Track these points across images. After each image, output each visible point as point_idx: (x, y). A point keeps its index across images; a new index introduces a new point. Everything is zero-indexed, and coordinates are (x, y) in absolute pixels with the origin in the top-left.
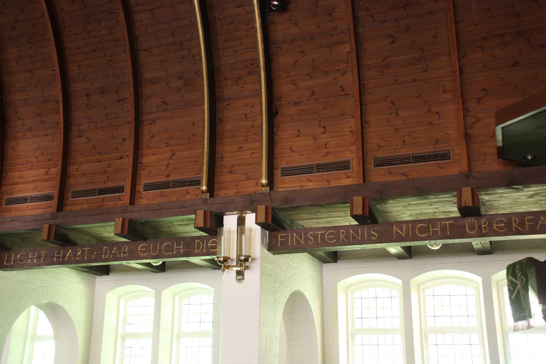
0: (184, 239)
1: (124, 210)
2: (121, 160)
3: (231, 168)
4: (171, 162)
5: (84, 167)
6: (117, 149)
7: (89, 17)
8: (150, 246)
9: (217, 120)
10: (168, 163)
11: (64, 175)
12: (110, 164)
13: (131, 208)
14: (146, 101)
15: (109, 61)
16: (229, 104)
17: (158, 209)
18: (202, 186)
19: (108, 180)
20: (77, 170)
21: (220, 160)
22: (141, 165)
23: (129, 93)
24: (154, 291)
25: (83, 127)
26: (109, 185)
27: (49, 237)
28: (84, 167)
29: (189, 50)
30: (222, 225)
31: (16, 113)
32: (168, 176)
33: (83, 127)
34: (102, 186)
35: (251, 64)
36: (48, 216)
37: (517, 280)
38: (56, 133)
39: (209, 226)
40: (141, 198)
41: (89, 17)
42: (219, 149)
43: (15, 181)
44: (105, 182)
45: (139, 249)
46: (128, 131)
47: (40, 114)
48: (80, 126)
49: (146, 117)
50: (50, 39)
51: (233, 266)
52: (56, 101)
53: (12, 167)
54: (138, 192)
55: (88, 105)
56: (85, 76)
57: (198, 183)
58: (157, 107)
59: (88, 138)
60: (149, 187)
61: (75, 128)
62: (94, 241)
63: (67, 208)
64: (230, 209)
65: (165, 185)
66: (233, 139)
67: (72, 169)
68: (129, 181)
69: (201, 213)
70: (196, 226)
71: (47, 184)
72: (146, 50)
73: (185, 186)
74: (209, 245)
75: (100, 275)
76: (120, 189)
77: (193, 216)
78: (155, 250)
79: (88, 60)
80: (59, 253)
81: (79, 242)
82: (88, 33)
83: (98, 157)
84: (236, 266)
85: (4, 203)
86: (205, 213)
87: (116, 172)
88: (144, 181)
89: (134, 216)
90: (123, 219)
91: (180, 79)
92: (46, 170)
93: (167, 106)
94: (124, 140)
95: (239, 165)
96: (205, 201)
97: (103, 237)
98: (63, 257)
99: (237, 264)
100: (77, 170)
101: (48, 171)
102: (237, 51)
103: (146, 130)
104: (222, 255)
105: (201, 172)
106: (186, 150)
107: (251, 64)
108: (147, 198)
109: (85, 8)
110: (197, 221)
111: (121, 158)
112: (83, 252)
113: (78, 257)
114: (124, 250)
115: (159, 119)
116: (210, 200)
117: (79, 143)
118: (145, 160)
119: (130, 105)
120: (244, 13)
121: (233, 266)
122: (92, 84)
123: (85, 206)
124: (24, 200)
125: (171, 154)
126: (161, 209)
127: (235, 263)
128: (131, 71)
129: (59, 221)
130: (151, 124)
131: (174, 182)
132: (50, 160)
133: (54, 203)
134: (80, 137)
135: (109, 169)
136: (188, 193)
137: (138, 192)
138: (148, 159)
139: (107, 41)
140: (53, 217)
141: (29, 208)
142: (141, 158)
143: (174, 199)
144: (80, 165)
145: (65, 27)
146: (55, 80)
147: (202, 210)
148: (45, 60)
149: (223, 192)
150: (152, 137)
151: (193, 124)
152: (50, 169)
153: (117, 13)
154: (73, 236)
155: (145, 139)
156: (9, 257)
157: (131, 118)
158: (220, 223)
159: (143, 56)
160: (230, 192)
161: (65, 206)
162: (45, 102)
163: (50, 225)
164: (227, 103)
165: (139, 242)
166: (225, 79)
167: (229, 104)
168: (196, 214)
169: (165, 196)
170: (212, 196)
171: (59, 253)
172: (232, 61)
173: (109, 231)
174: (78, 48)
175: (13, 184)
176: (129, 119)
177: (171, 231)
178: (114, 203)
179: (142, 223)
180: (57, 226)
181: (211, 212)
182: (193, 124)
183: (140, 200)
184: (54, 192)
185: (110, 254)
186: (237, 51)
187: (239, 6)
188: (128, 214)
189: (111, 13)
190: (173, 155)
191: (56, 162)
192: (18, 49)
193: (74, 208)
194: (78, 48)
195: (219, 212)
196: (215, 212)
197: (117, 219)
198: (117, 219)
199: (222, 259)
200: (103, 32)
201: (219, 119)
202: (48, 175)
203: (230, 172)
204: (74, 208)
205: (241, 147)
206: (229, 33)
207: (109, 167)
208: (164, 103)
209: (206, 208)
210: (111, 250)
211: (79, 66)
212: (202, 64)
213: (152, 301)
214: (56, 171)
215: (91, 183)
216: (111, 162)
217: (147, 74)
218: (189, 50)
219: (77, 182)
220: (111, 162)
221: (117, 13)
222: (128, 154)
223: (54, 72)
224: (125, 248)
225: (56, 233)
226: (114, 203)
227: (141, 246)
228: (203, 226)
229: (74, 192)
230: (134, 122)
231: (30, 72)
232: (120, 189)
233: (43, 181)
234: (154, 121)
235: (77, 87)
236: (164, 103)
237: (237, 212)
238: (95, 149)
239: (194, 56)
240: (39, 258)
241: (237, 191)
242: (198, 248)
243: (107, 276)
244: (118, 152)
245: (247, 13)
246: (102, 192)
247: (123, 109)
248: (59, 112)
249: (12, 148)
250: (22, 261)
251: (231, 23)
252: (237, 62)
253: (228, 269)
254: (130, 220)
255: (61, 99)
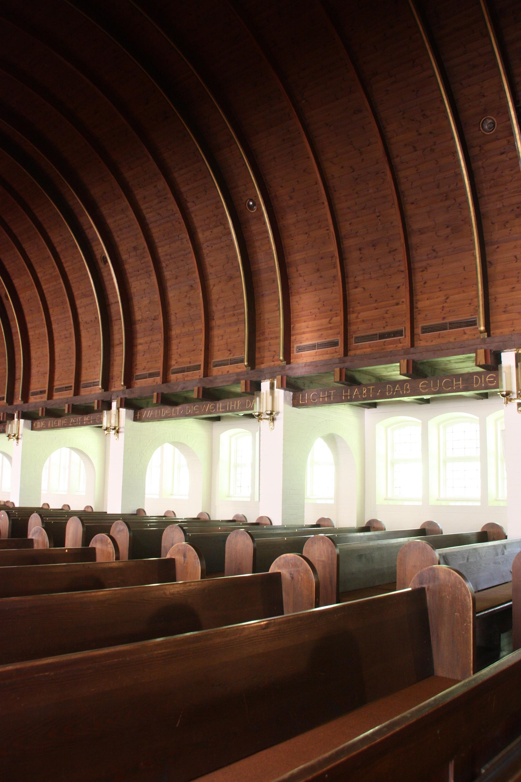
0: (462, 375)
1: (406, 352)
2: (397, 307)
3: (505, 308)
4: (445, 305)
5: (363, 315)
6: (392, 296)
7: (357, 179)
8: (430, 383)
9: (488, 263)
10: (443, 307)
11: (346, 323)
12: (387, 310)
13: (412, 350)
14: (416, 250)
15: (379, 216)
16: (498, 247)
17: (439, 350)
18: (480, 327)
19: (387, 325)
20: (357, 317)
21: (494, 301)
22: (417, 310)
23: (399, 244)
24: (421, 421)
25: (359, 278)
26: (388, 329)
27: (341, 379)
28: (363, 315)
29: (455, 200)
30: (500, 362)
31: (297, 271)
32: (444, 318)
33: (359, 278)
34: (382, 331)
35: (518, 208)
36: (337, 361)
37: (327, 536)
38: (334, 286)
39: (489, 363)
40: (420, 340)
41: (357, 179)
42: (491, 291)
43: (303, 331)
44: (384, 327)
45: (420, 386)
46: (402, 279)
47: (318, 270)
48: (355, 277)
49: (417, 265)
50: (323, 203)
51: (515, 399)
52: (332, 257)
53: (297, 319)
54: (416, 334)
55: (361, 258)
56: (357, 232)
57: (474, 323)
58: (428, 255)
59: (364, 288)
60: (425, 330)
61: (351, 279)
62: (374, 381)
63: (351, 353)
64: (507, 347)
65: (442, 327)
66: (505, 280)
67: (352, 317)
68: (408, 325)
69: (481, 352)
70: (478, 364)
71: (331, 332)
72: (412, 203)
73: (461, 327)
74: (487, 380)
75: (368, 408)
76: (399, 333)
77: (474, 355)
78: (435, 385)
79: (358, 217)
80: (346, 392)
81: (364, 382)
82: (357, 193)
83: (375, 305)
84: (518, 398)
85: (295, 351)
86: (485, 351)
87: (394, 317)
88: (420, 324)
89: (415, 357)
90: (407, 361)
91: (448, 227)
92: (328, 320)
93: (437, 253)
94: (399, 287)
95: (513, 305)
96: (484, 340)
97: (381, 376)
98: (351, 396)
99: (518, 397)
100: (357, 317)
101: (330, 320)
102: (502, 196)
103: (418, 277)
104: (505, 390)
105: (477, 311)
106: (459, 293)
107: (518, 208)
108: (425, 341)
109: (353, 172)
110: (479, 360)
111: (397, 304)
112: (368, 390)
113: (364, 395)
114: (406, 387)
115: (431, 266)
116: (488, 340)
117: (355, 293)
118: (420, 305)
119: (401, 255)
120: (508, 159)
121: (515, 399)
122: (364, 239)
123: (368, 350)
124: (313, 347)
125: (444, 298)
126: (442, 350)
127: (515, 396)
128: (401, 225)
129: (347, 365)
130: (422, 271)
131: (450, 323)
132: (331, 310)
133: (340, 348)
134: (356, 288)
135: (386, 315)
136: (465, 333)
137: (416, 334)
138: (422, 304)
139: (375, 199)
140: (341, 361)
141: (317, 353)
142: (416, 303)
143: (452, 340)
144: (359, 313)
145: (335, 191)
146: (329, 238)
147: (481, 348)
148: (319, 222)
149: (498, 331)
150: (425, 283)
151: (464, 268)
152: (332, 318)
153: (383, 172)
154: (358, 376)
155: (418, 286)
156: (303, 396)
157: (404, 266)
158: (498, 360)
159: (410, 210)
160: (506, 330)
161: (350, 350)
162: (322, 258)
163: (340, 369)
164: (496, 246)
165: (420, 380)
166: (493, 223)
167: (498, 247)
168: (476, 353)
169: (443, 337)
170: (489, 335)
171: (346, 392)
172: (498, 206)
173: (394, 371)
174: (349, 208)
175: (297, 334)
176: (402, 268)
177: (446, 368)
178: (395, 346)
179: (422, 363)
180: (346, 369)
181: (491, 350)
182: (464, 268)
183: (419, 342)
184: (340, 339)
185: (394, 391)
186: (502, 196)
187: (502, 154)
188: (411, 355)
189: (377, 173)
190: (447, 298)
191: (339, 312)
192: (296, 215)
193: (358, 352)
194: (349, 208)
195: (498, 349)
196: (494, 350)
197: (402, 361)
198: (402, 361)
199: (504, 393)
200: (371, 191)
201: (490, 262)
202: (330, 323)
203: (504, 312)
204: (358, 352)
205: (514, 288)
206: (493, 179)
207: (387, 313)
208: (434, 250)
209: (485, 346)
210: (394, 387)
211: (350, 224)
212: (470, 212)
213: (418, 430)
214: (339, 319)
215: (371, 329)
216: (388, 308)
217: (415, 225)
218: (455, 200)
219: (359, 329)
220: (388, 308)
221: (383, 172)
222: (404, 300)
223: (328, 232)
224: (407, 385)
225: (346, 376)
226: (395, 346)
227: (422, 383)
228: (484, 363)
229: (356, 338)
230: (407, 271)
231: (306, 233)
232: (399, 333)
233: (326, 329)
234: (426, 268)
235: (349, 243)
236: (434, 250)
237: (515, 349)
238: (371, 297)
239: (460, 205)
240: (329, 396)
241: (512, 329)
242: (477, 383)
243: (374, 409)
244: (394, 299)
245: (510, 159)
246: (382, 336)
247: (394, 259)
248: (335, 267)
249: (297, 302)
250: (314, 400)
251: (495, 170)
252: (503, 206)
253: (510, 401)
254: (414, 361)
255: (337, 254)
